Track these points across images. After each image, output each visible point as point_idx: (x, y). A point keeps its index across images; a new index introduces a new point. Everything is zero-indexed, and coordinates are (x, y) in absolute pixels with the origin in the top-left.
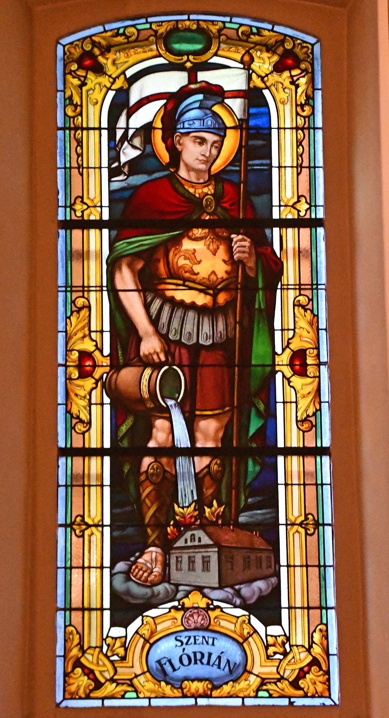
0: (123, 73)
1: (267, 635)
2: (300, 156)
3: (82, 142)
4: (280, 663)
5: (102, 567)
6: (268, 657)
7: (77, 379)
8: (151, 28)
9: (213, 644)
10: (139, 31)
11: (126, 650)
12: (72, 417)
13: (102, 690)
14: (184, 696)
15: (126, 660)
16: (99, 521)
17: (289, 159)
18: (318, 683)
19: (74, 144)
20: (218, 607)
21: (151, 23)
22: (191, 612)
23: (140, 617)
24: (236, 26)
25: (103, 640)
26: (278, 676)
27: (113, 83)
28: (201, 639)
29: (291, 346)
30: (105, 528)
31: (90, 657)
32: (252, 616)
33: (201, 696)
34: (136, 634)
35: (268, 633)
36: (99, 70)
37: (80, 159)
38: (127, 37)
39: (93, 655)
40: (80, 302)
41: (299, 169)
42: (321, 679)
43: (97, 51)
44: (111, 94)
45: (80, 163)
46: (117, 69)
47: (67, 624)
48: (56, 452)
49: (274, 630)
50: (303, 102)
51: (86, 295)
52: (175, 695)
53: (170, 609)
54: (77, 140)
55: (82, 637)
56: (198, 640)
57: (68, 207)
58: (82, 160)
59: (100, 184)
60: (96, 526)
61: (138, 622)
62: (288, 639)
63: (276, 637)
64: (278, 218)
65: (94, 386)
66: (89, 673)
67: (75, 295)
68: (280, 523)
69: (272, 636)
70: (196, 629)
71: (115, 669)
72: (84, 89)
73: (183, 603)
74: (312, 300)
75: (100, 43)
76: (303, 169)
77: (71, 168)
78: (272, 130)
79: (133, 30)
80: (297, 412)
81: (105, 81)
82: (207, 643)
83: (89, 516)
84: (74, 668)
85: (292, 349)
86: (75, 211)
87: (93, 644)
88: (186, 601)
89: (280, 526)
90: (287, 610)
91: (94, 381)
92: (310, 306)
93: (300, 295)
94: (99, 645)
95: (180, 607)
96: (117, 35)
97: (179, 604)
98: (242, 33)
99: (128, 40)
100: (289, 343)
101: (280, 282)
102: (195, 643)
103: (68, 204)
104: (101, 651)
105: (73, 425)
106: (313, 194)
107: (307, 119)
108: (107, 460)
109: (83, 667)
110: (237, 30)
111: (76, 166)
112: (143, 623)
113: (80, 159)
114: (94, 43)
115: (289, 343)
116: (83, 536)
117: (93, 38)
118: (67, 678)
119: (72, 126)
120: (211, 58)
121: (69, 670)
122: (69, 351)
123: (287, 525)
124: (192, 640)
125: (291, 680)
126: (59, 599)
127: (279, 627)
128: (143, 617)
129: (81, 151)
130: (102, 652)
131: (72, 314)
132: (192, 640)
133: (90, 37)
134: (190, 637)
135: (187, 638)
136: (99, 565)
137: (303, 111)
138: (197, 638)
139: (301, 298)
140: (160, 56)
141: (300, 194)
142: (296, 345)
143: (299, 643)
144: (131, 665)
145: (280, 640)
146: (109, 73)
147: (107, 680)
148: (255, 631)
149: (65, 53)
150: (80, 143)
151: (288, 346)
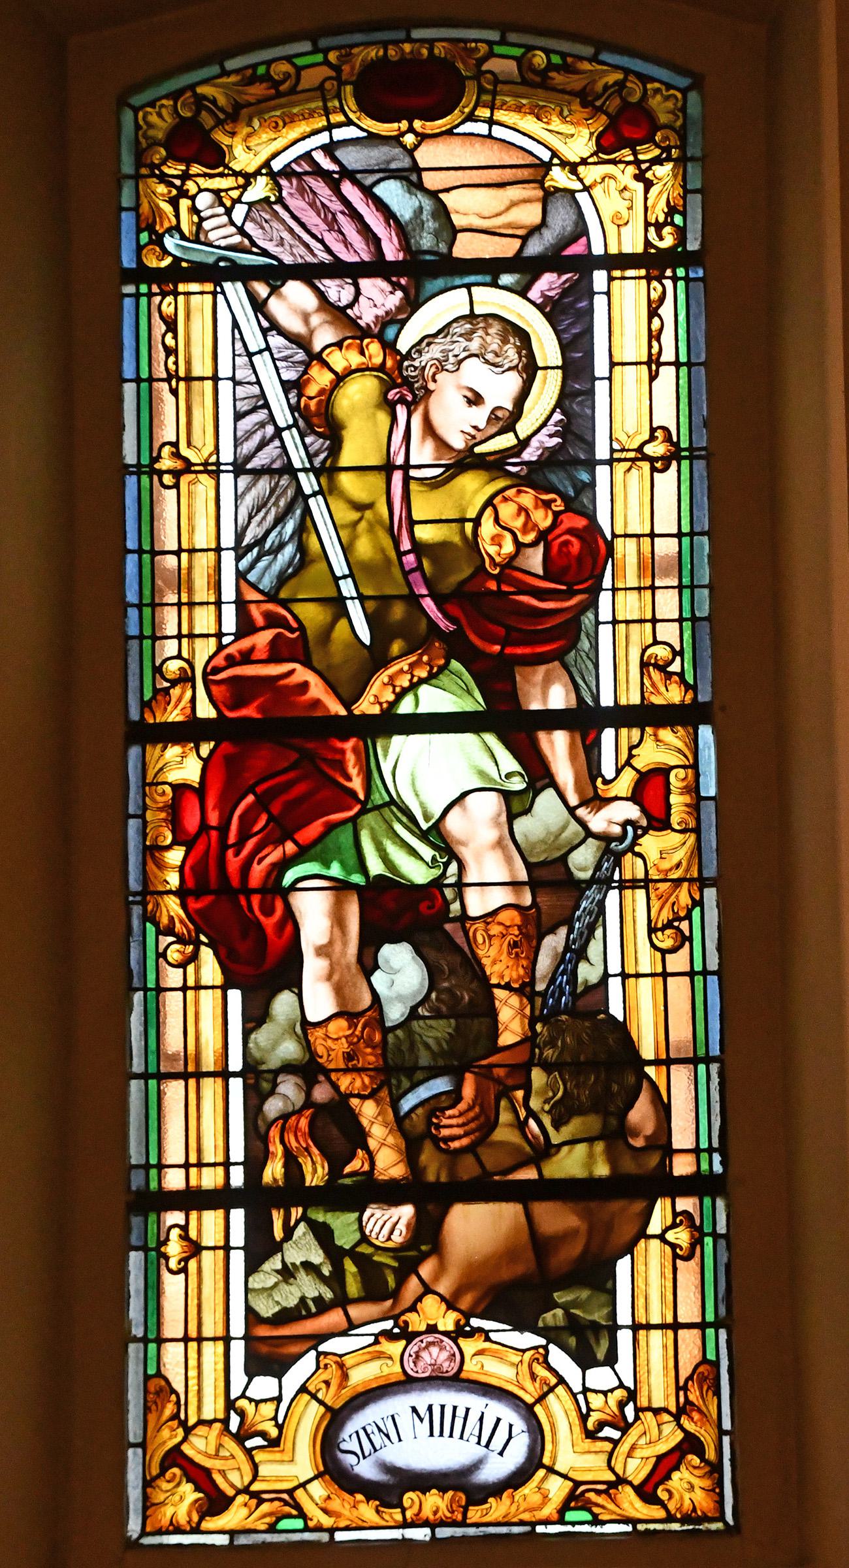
0: (267, 164)
2: (654, 336)
5: (227, 1248)
10: (299, 69)
11: (280, 1427)
15: (278, 1446)
17: (633, 346)
19: (160, 327)
20: (480, 1330)
22: (422, 1341)
25: (230, 1405)
26: (611, 1477)
29: (634, 762)
32: (552, 1347)
33: (443, 1523)
36: (216, 159)
37: (172, 359)
38: (276, 84)
41: (654, 367)
42: (707, 1483)
43: (207, 120)
45: (172, 367)
47: (151, 1371)
48: (121, 730)
49: (600, 1377)
50: (661, 219)
52: (384, 1523)
53: (377, 1336)
55: (183, 1402)
58: (176, 363)
59: (220, 1020)
61: (308, 1363)
62: (632, 1395)
63: (605, 1393)
66: (200, 1476)
73: (406, 1323)
74: (681, 653)
75: (214, 101)
76: (662, 369)
77: (151, 380)
78: (597, 383)
79: (285, 67)
80: (646, 199)
84: (164, 1469)
85: (638, 767)
87: (208, 1415)
88: (411, 1317)
92: (675, 667)
94: (221, 1416)
95: (396, 1330)
96: (253, 80)
97: (396, 1325)
108: (238, 1216)
111: (164, 375)
112: (318, 1368)
114: (200, 100)
115: (631, 756)
118: (149, 1490)
121: (155, 1471)
122: (151, 784)
126: (135, 1061)
128: (319, 1354)
129: (172, 309)
130: (230, 1432)
133: (192, 87)
136: (220, 1159)
137: (661, 238)
140: (349, 123)
145: (613, 1399)
148: (561, 1381)
149: (138, 127)
150: (171, 325)
151: (628, 763)
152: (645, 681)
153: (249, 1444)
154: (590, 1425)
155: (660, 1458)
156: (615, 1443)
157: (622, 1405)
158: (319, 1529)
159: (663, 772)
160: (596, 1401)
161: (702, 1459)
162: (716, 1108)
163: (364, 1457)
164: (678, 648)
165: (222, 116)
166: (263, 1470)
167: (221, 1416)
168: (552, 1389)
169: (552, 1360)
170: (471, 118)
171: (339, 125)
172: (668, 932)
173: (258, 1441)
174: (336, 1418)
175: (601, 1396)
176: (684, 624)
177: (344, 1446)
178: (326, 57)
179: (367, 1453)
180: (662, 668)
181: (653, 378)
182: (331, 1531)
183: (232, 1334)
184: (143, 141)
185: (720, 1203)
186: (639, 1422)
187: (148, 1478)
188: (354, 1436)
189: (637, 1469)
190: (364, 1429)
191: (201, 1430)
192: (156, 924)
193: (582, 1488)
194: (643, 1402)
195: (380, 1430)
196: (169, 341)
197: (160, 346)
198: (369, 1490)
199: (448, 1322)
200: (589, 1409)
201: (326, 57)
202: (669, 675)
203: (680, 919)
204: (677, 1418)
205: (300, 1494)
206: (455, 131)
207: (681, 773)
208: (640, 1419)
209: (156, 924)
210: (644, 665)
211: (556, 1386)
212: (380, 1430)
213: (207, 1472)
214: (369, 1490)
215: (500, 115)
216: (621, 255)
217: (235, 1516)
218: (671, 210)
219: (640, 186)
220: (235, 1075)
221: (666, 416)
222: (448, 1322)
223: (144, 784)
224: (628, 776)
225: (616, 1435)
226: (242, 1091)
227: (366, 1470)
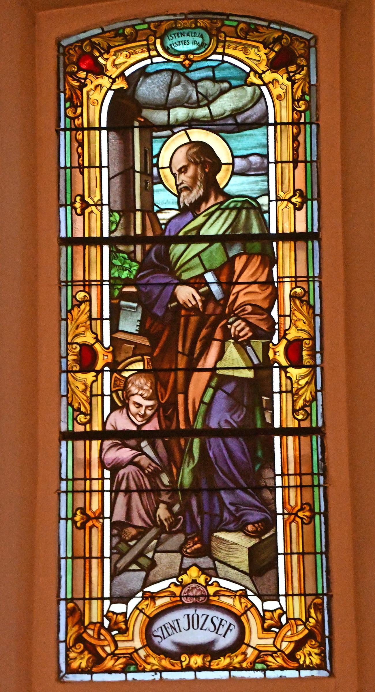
0: (122, 74)
1: (264, 611)
2: (295, 150)
6: (264, 630)
7: (107, 641)
8: (149, 28)
12: (74, 410)
14: (183, 670)
18: (313, 655)
19: (76, 145)
21: (149, 23)
24: (235, 24)
25: (103, 616)
29: (287, 337)
30: (105, 520)
31: (91, 632)
34: (135, 609)
39: (94, 630)
40: (80, 296)
42: (316, 651)
44: (111, 93)
45: (81, 162)
46: (117, 69)
48: (57, 435)
49: (271, 605)
51: (87, 290)
54: (77, 141)
57: (68, 205)
58: (83, 160)
65: (95, 378)
67: (77, 289)
68: (274, 391)
69: (269, 611)
71: (115, 643)
81: (105, 82)
83: (90, 509)
86: (76, 209)
89: (279, 556)
92: (305, 298)
93: (297, 287)
94: (99, 620)
98: (241, 30)
100: (285, 334)
103: (69, 203)
105: (74, 294)
107: (303, 114)
109: (84, 641)
110: (236, 27)
111: (77, 165)
113: (81, 159)
117: (93, 40)
119: (73, 127)
120: (210, 55)
125: (287, 652)
127: (277, 602)
130: (104, 627)
131: (73, 308)
139: (298, 290)
141: (296, 188)
142: (292, 335)
144: (131, 638)
145: (276, 615)
146: (109, 74)
147: (108, 655)
152: (292, 303)
153: (113, 633)
154: (266, 625)
156: (277, 633)
157: (280, 616)
159: (298, 342)
160: (268, 615)
161: (316, 641)
163: (165, 638)
165: (103, 51)
166: (120, 644)
168: (249, 609)
170: (215, 53)
171: (155, 56)
173: (116, 632)
174: (152, 620)
175: (270, 613)
177: (155, 634)
178: (149, 26)
179: (165, 637)
180: (300, 298)
181: (295, 168)
183: (103, 165)
184: (67, 61)
186: (288, 624)
187: (69, 647)
188: (160, 629)
190: (164, 626)
192: (73, 407)
193: (262, 653)
195: (171, 626)
196: (80, 150)
197: (76, 153)
198: (167, 654)
201: (149, 26)
202: (302, 302)
206: (208, 58)
207: (307, 341)
208: (289, 623)
209: (73, 407)
210: (291, 297)
211: (250, 608)
212: (171, 626)
213: (94, 646)
214: (167, 654)
215: (227, 51)
216: (284, 234)
218: (304, 93)
219: (290, 83)
220: (107, 599)
221: (300, 185)
223: (68, 343)
224: (284, 342)
225: (277, 630)
226: (110, 402)
227: (167, 644)
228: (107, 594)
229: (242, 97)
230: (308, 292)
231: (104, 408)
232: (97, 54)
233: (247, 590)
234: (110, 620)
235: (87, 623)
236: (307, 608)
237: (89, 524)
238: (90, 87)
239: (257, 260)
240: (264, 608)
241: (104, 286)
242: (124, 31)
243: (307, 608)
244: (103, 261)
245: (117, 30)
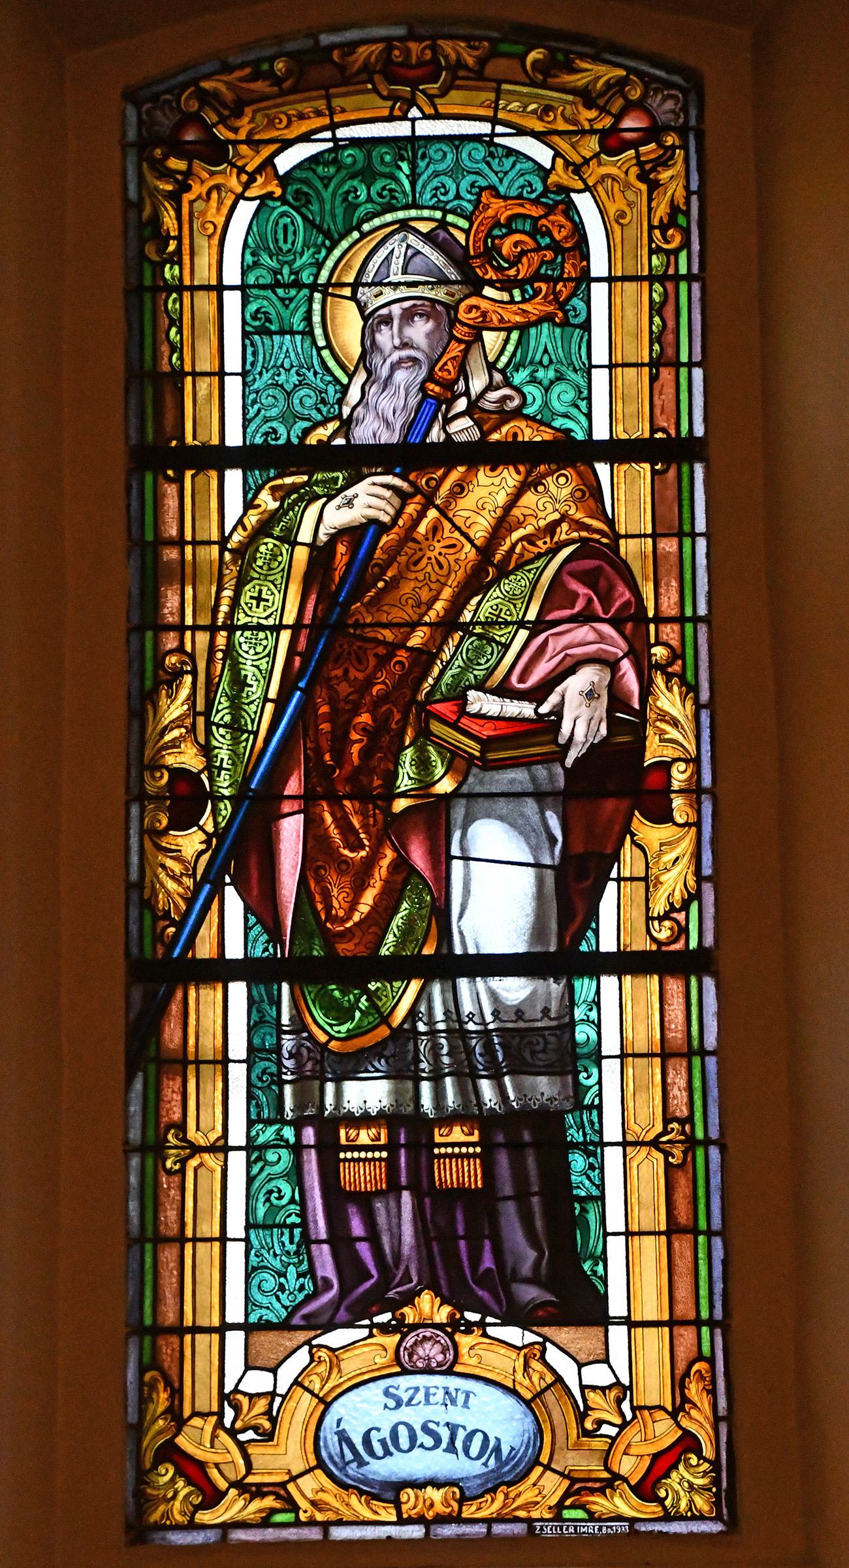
1: (583, 1388)
3: (181, 319)
4: (611, 1446)
9: (466, 1404)
11: (274, 1421)
13: (217, 1510)
16: (218, 1139)
23: (306, 1348)
25: (223, 1397)
27: (246, 186)
28: (441, 1393)
35: (584, 1383)
43: (211, 117)
49: (597, 1375)
56: (434, 1395)
58: (181, 358)
60: (212, 1149)
64: (606, 437)
69: (594, 1388)
70: (428, 1371)
71: (247, 1458)
72: (187, 197)
82: (454, 1402)
90: (605, 285)
91: (204, 837)
92: (676, 668)
99: (280, 88)
101: (616, 864)
102: (427, 1402)
104: (220, 1424)
106: (647, 1195)
107: (672, 258)
112: (312, 1361)
113: (175, 357)
116: (182, 1172)
123: (611, 366)
124: (420, 1396)
128: (312, 1347)
132: (420, 1396)
134: (417, 1389)
135: (411, 1392)
138: (432, 1391)
143: (653, 1400)
148: (559, 1379)
149: (140, 123)
153: (242, 1437)
155: (655, 1457)
158: (312, 1523)
160: (594, 1398)
161: (700, 1456)
162: (714, 1093)
164: (679, 651)
166: (256, 1463)
167: (215, 1408)
169: (548, 1357)
172: (667, 923)
173: (250, 1435)
176: (707, 1058)
182: (326, 1526)
185: (709, 983)
189: (629, 1466)
191: (197, 1422)
194: (640, 1401)
199: (442, 1315)
200: (587, 1407)
202: (669, 678)
203: (678, 911)
204: (674, 1415)
205: (291, 1487)
207: (682, 766)
213: (202, 1465)
217: (233, 1508)
219: (644, 187)
222: (442, 1315)
228: (235, 1314)
229: (551, 817)
230: (683, 657)
231: (229, 1178)
232: (214, 118)
233: (548, 1344)
234: (237, 1408)
235: (187, 1412)
236: (678, 1377)
237: (193, 1163)
238: (197, 189)
239: (594, 1503)
240: (584, 1383)
241: (231, 1065)
242: (272, 66)
243: (678, 1377)
244: (228, 1205)
245: (256, 64)
